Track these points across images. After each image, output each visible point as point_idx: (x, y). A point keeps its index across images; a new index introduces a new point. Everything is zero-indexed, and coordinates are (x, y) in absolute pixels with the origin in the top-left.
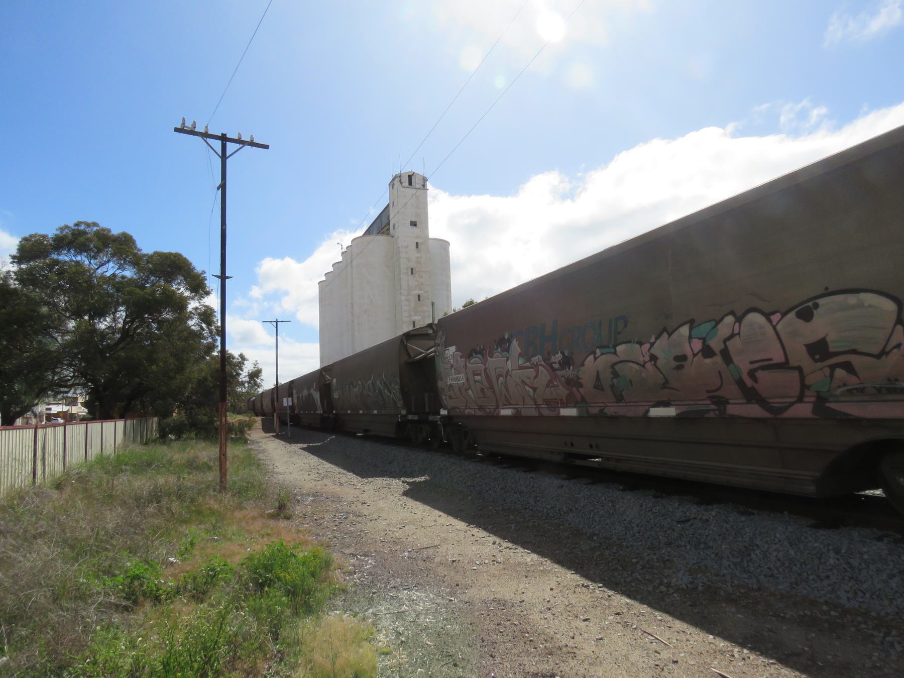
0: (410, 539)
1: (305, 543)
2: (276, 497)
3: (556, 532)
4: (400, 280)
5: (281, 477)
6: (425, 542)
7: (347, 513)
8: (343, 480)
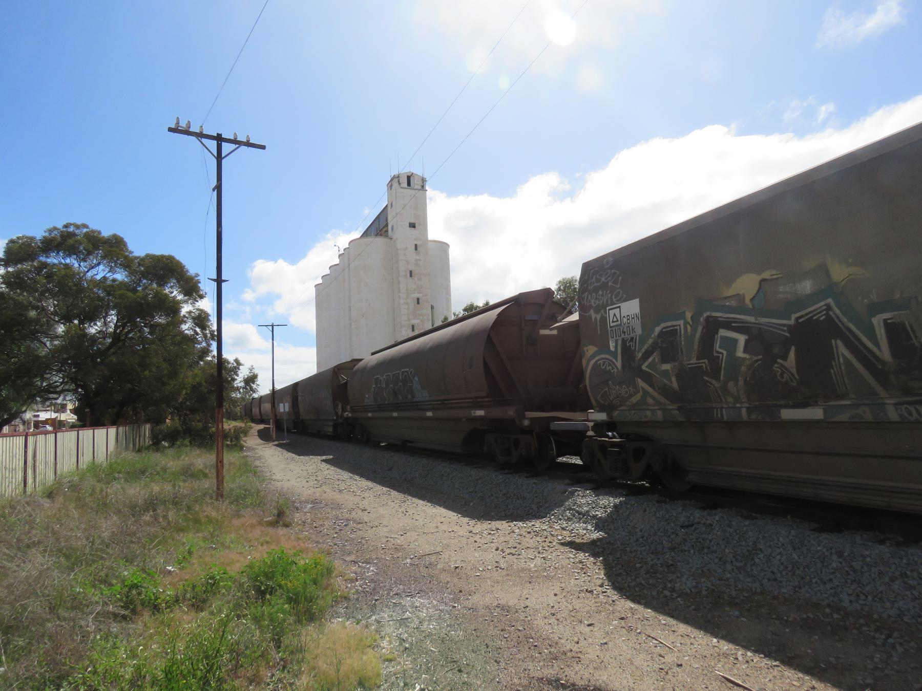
0: (412, 546)
1: (306, 550)
2: (274, 504)
4: (399, 282)
5: (279, 484)
6: (428, 549)
7: (348, 520)
8: (342, 487)
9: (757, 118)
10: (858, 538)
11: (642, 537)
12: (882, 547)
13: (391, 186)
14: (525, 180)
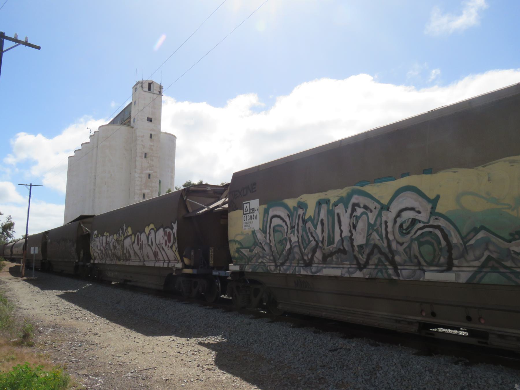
0: (133, 363)
1: (47, 365)
3: (245, 357)
4: (136, 161)
6: (145, 365)
7: (82, 342)
9: (389, 73)
10: (442, 360)
11: (303, 358)
12: (457, 366)
13: (136, 89)
14: (234, 96)
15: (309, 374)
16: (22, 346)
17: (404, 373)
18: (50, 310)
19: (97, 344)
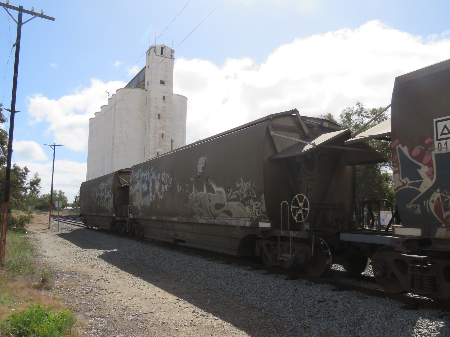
1: (59, 307)
3: (238, 306)
4: (150, 122)
7: (93, 287)
8: (94, 263)
11: (292, 308)
13: (149, 53)
15: (296, 323)
16: (41, 290)
17: (387, 325)
18: (69, 259)
19: (106, 289)
